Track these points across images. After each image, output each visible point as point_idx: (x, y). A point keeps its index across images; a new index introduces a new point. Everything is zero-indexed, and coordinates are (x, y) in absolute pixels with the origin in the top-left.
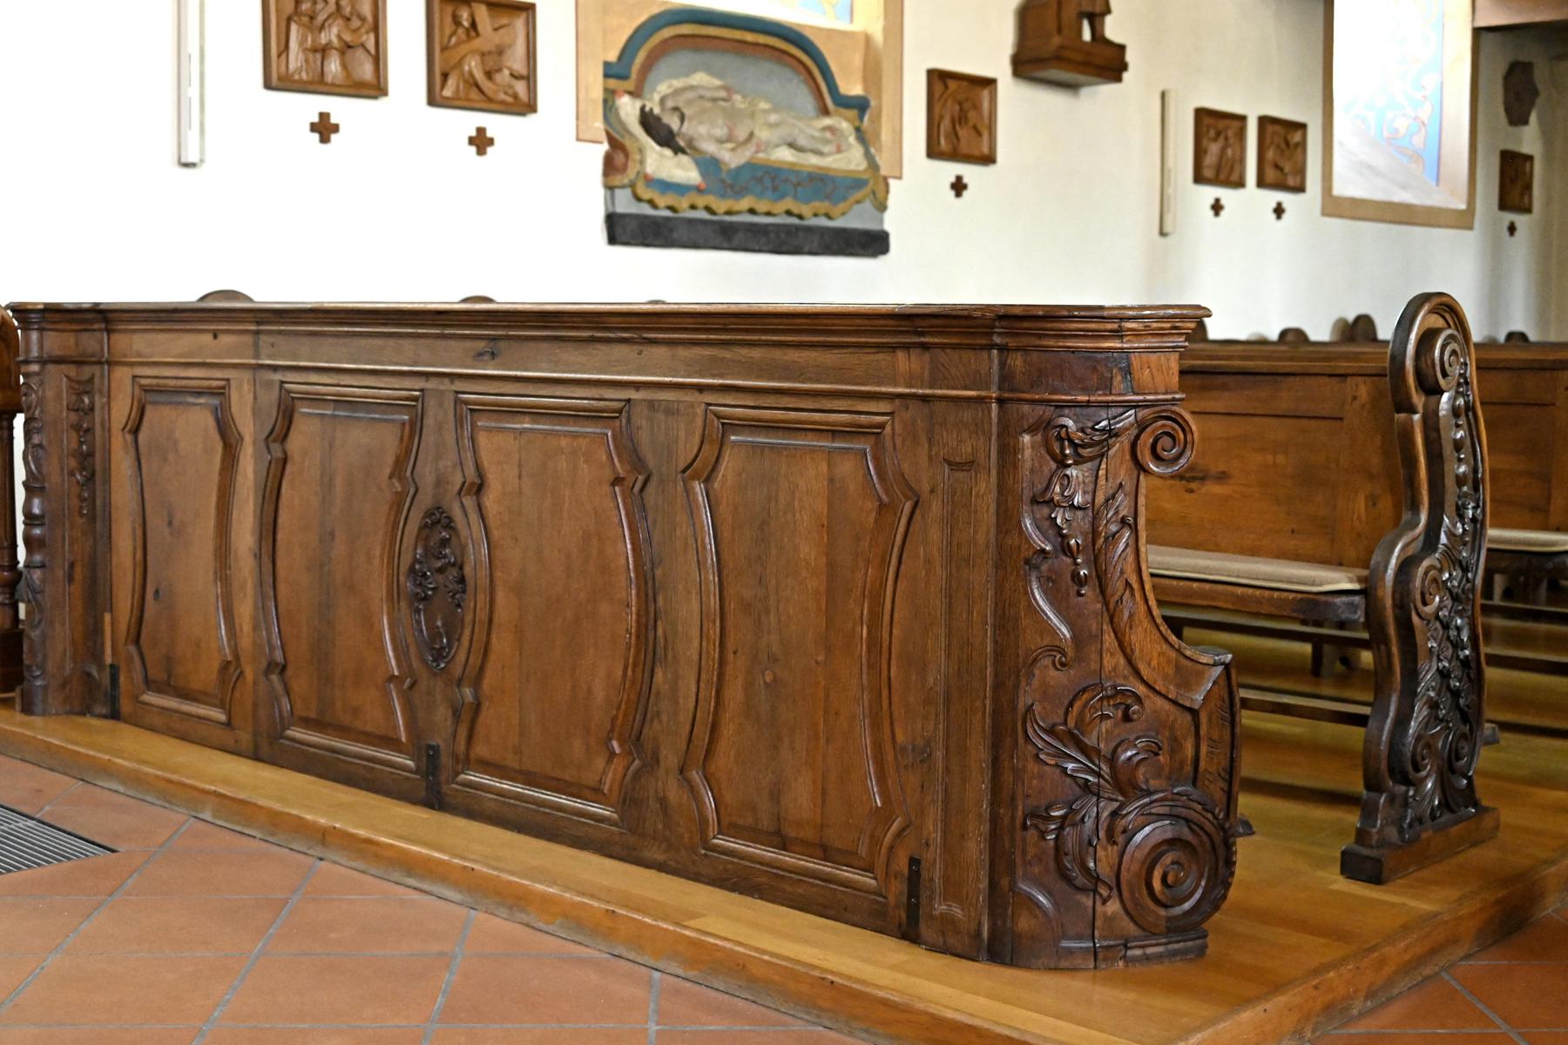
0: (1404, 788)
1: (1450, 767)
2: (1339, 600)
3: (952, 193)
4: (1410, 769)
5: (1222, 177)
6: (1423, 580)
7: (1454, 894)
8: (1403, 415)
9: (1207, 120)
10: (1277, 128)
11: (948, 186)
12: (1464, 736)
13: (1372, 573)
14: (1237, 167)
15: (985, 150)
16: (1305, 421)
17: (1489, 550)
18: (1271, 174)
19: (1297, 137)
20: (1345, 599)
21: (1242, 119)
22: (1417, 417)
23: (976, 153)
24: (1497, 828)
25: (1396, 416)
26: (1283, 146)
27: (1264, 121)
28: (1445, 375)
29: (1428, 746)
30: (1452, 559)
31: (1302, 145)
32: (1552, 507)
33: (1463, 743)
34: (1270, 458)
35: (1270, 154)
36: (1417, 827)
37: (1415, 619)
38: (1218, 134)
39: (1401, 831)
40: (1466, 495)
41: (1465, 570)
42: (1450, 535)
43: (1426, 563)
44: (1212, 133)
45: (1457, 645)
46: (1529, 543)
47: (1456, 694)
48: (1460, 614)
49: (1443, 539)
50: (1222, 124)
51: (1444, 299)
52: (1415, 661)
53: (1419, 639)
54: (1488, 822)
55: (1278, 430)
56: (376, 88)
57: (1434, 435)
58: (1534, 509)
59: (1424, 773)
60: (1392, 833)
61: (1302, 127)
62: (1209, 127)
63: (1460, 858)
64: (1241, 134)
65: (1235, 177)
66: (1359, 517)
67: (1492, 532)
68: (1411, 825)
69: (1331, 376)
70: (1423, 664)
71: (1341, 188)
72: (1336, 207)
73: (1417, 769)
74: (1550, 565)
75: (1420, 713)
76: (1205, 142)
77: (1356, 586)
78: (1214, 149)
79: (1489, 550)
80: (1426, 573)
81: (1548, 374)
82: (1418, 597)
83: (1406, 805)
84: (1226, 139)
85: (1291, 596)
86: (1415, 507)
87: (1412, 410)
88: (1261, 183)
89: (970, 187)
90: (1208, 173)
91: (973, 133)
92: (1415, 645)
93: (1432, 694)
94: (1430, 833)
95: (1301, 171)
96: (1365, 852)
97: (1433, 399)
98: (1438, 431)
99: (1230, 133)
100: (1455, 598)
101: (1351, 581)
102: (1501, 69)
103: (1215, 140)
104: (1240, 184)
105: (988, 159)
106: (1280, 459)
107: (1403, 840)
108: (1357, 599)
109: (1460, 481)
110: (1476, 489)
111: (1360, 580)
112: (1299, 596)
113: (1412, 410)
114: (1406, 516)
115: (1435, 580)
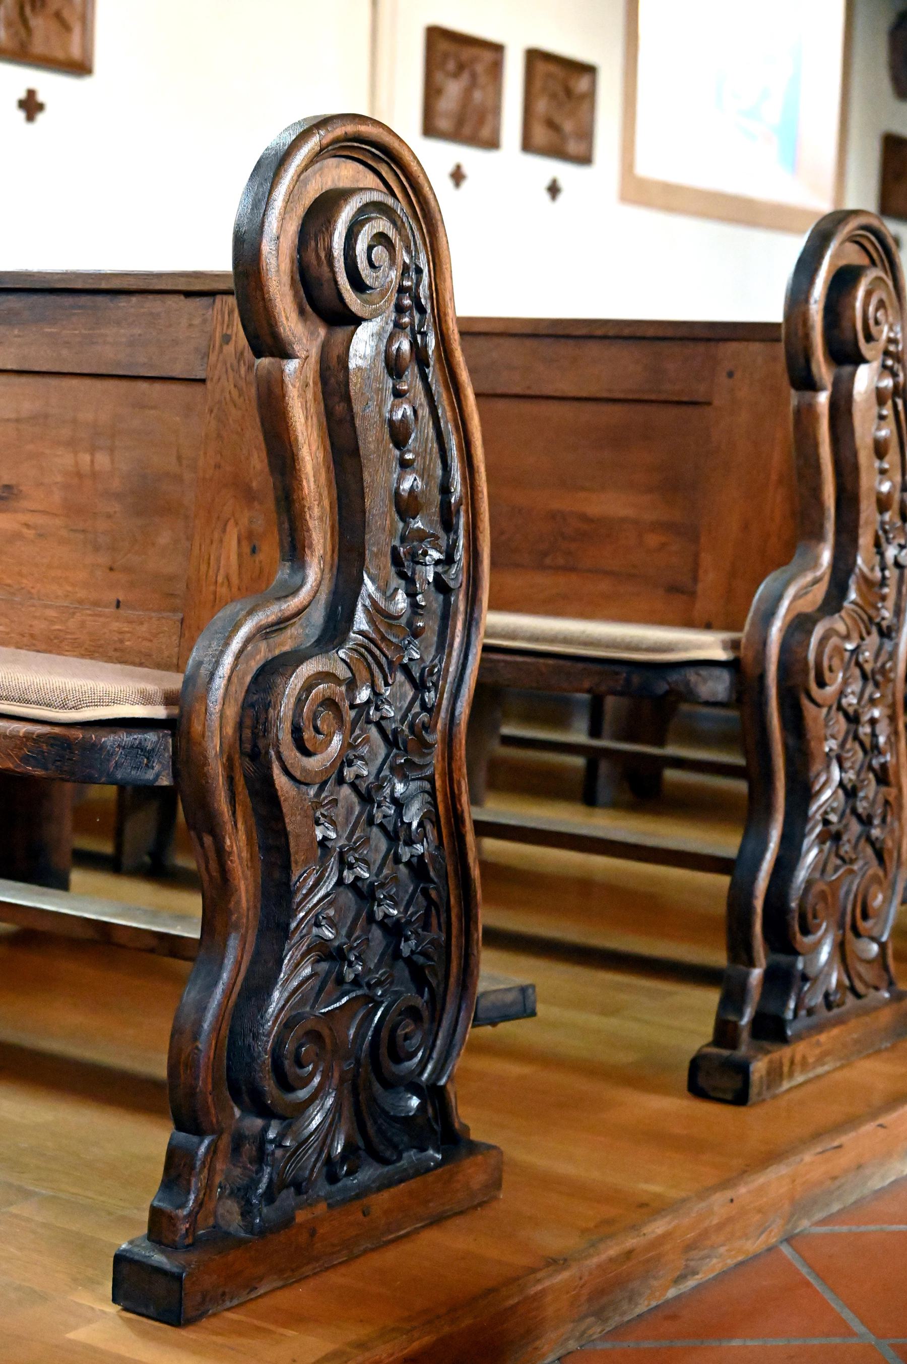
0: (259, 1122)
1: (372, 1073)
2: (110, 739)
3: (21, 115)
4: (269, 1085)
5: (467, 130)
6: (300, 702)
7: (354, 1333)
8: (265, 361)
9: (443, 46)
10: (552, 68)
11: (14, 104)
12: (413, 1013)
13: (188, 682)
14: (490, 117)
15: (76, 52)
16: (144, 386)
17: (486, 648)
18: (541, 135)
19: (582, 84)
20: (126, 737)
21: (498, 49)
22: (291, 366)
23: (60, 55)
24: (496, 1184)
25: (258, 361)
26: (561, 94)
27: (534, 57)
28: (359, 285)
29: (315, 1036)
30: (378, 659)
31: (590, 96)
32: (700, 587)
33: (408, 1027)
34: (85, 458)
35: (542, 106)
36: (287, 1197)
37: (281, 780)
38: (461, 67)
39: (247, 1212)
40: (421, 536)
41: (420, 686)
42: (377, 613)
43: (307, 669)
44: (451, 66)
45: (396, 834)
46: (567, 640)
47: (394, 931)
48: (401, 772)
49: (361, 622)
50: (467, 53)
51: (365, 129)
52: (287, 868)
53: (293, 823)
54: (473, 1173)
55: (98, 403)
56: (492, 143)
57: (340, 408)
58: (674, 589)
59: (303, 1094)
60: (230, 1214)
61: (589, 70)
62: (446, 56)
63: (389, 1257)
64: (496, 69)
65: (485, 133)
66: (227, 577)
67: (492, 619)
68: (270, 1197)
69: (188, 294)
70: (303, 875)
71: (644, 168)
72: (638, 191)
73: (286, 1085)
74: (662, 687)
75: (296, 972)
76: (439, 77)
77: (159, 712)
78: (453, 90)
79: (486, 648)
80: (308, 687)
81: (701, 348)
82: (285, 735)
83: (261, 1157)
84: (474, 76)
85: (23, 728)
86: (295, 550)
87: (283, 352)
88: (527, 146)
89: (49, 108)
90: (443, 124)
91: (54, 26)
92: (285, 834)
93: (328, 934)
94: (321, 1208)
95: (587, 135)
96: (158, 1258)
97: (340, 333)
98: (347, 398)
99: (480, 68)
100: (391, 741)
101: (147, 699)
102: (884, 22)
103: (456, 75)
104: (492, 143)
105: (80, 68)
106: (103, 460)
107: (249, 1228)
108: (151, 737)
109: (406, 506)
110: (448, 525)
111: (169, 699)
112: (23, 728)
113: (283, 352)
114: (283, 572)
115: (329, 703)
